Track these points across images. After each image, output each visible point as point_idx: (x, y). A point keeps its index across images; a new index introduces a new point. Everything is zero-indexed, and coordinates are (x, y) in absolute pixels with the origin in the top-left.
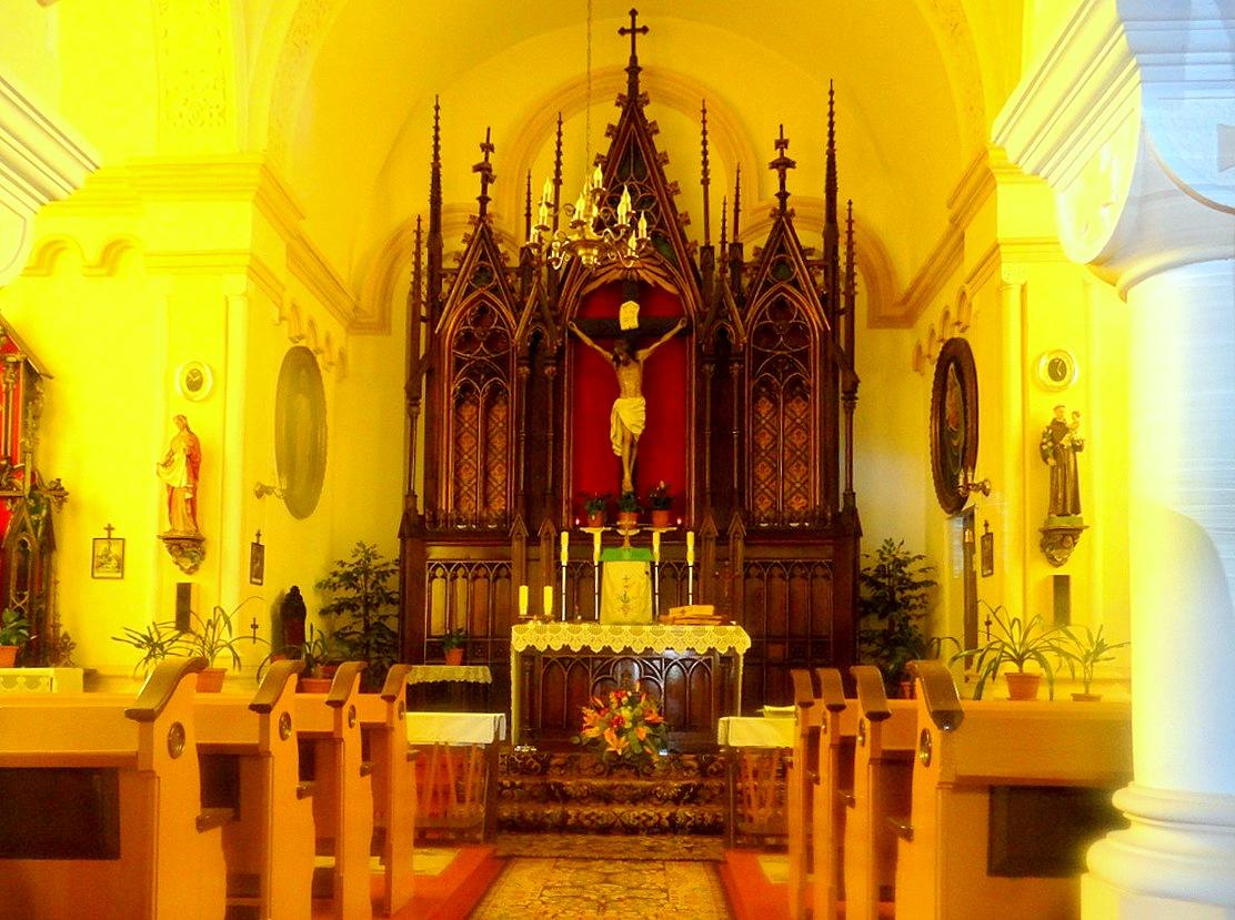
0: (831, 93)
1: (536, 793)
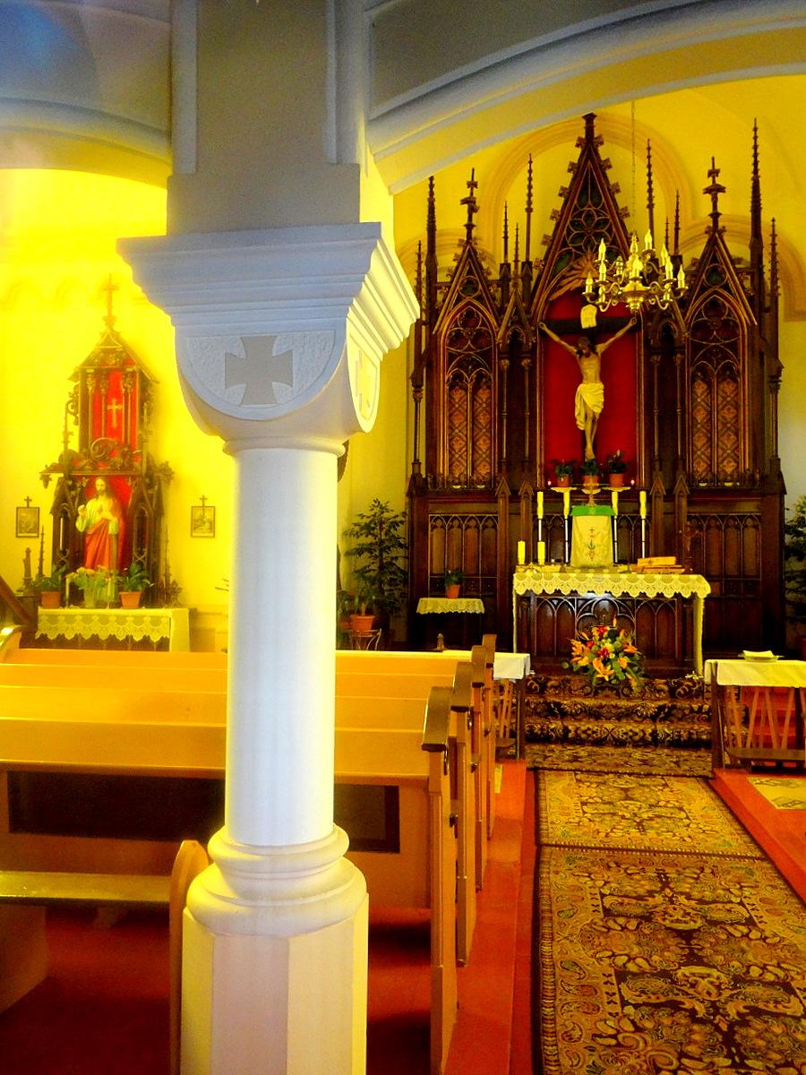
0: (755, 129)
1: (538, 710)
